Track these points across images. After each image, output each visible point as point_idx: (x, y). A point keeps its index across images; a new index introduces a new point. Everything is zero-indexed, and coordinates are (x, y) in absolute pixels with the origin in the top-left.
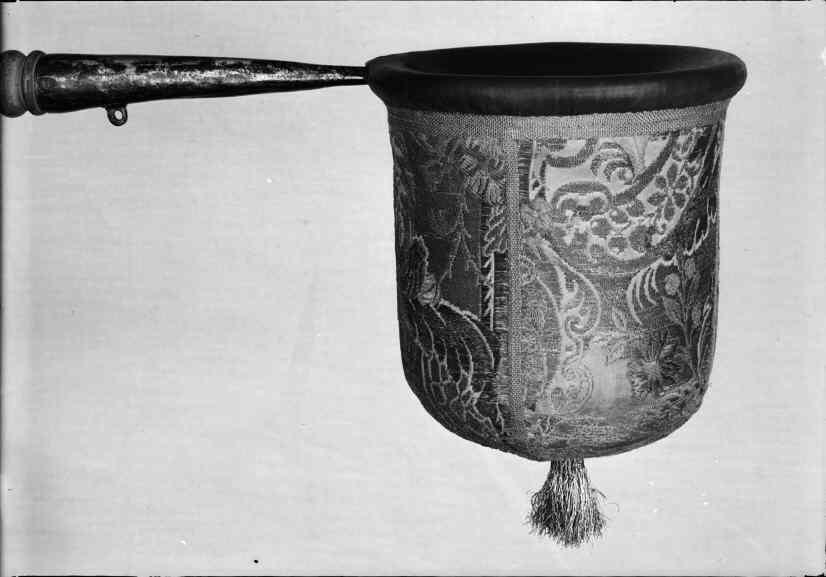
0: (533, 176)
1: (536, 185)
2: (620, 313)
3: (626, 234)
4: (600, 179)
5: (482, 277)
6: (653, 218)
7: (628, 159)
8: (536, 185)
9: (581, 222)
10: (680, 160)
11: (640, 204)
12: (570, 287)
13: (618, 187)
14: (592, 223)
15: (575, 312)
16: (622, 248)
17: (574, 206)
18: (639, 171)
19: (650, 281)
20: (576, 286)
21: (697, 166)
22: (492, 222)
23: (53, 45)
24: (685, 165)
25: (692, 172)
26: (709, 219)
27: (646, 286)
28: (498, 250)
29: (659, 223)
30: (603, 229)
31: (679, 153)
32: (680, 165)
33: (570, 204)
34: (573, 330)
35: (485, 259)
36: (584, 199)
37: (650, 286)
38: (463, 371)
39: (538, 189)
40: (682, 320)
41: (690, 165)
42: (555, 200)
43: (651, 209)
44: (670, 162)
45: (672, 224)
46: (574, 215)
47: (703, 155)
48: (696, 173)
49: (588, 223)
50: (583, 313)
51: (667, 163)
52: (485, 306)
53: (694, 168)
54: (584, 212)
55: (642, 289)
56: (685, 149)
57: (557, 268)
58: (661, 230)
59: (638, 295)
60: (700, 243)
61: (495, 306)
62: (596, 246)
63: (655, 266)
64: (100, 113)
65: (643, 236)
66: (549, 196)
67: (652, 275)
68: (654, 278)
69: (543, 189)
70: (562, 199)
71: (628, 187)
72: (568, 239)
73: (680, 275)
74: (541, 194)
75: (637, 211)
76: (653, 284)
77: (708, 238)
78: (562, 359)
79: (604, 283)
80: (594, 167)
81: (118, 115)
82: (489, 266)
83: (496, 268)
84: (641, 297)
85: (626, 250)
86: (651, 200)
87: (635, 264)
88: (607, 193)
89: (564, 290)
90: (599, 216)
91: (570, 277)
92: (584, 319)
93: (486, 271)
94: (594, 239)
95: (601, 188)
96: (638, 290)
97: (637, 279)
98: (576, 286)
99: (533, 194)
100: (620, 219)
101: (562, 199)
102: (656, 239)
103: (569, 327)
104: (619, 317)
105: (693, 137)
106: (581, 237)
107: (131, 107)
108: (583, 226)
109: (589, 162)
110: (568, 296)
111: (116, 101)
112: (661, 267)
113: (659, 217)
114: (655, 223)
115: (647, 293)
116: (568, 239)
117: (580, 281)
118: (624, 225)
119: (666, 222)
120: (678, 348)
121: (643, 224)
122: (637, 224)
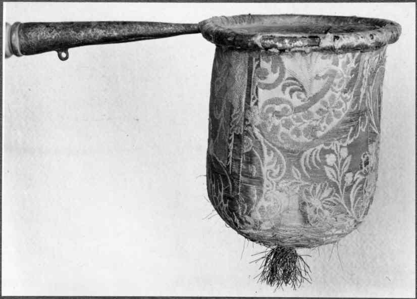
0: (253, 94)
1: (254, 99)
2: (297, 170)
3: (302, 128)
4: (287, 96)
5: (228, 144)
6: (319, 122)
7: (302, 87)
8: (254, 99)
9: (276, 120)
10: (337, 92)
11: (310, 114)
12: (269, 154)
13: (296, 102)
14: (282, 120)
15: (272, 167)
16: (298, 135)
17: (273, 111)
18: (309, 95)
19: (316, 155)
20: (272, 154)
21: (349, 97)
22: (234, 116)
23: (4, 6)
24: (341, 96)
25: (346, 100)
26: (360, 128)
27: (313, 158)
28: (236, 132)
29: (322, 125)
30: (287, 125)
31: (336, 88)
32: (337, 95)
33: (270, 110)
34: (270, 176)
35: (230, 135)
36: (278, 108)
37: (316, 159)
38: (219, 192)
39: (255, 101)
40: (337, 180)
41: (344, 96)
42: (263, 107)
43: (317, 116)
44: (330, 93)
45: (329, 128)
46: (273, 116)
47: (352, 91)
48: (348, 101)
49: (280, 121)
50: (276, 168)
51: (328, 93)
52: (228, 160)
53: (346, 98)
54: (278, 115)
55: (310, 159)
56: (339, 86)
57: (263, 144)
58: (323, 129)
59: (307, 161)
60: (352, 140)
61: (232, 161)
62: (283, 134)
63: (319, 148)
64: (54, 54)
65: (312, 131)
66: (260, 104)
67: (316, 153)
68: (318, 155)
69: (257, 101)
70: (265, 109)
71: (303, 103)
72: (269, 129)
73: (336, 155)
74: (256, 104)
75: (309, 116)
76: (319, 159)
77: (358, 138)
78: (264, 191)
79: (288, 153)
80: (283, 90)
81: (64, 55)
82: (232, 139)
83: (234, 141)
84: (316, 164)
85: (300, 137)
86: (318, 112)
87: (308, 145)
88: (291, 105)
89: (266, 155)
90: (285, 117)
91: (269, 149)
92: (276, 172)
93: (230, 141)
94: (282, 129)
95: (289, 102)
96: (308, 159)
97: (308, 153)
98: (272, 154)
99: (252, 103)
100: (298, 120)
101: (265, 109)
102: (320, 134)
103: (268, 174)
104: (296, 172)
105: (345, 80)
106: (275, 128)
107: (70, 50)
108: (277, 122)
109: (280, 87)
110: (267, 159)
111: (62, 47)
112: (322, 149)
113: (322, 122)
114: (319, 124)
115: (314, 162)
116: (269, 129)
117: (274, 151)
118: (300, 123)
119: (326, 125)
120: (333, 194)
121: (311, 124)
122: (308, 123)
